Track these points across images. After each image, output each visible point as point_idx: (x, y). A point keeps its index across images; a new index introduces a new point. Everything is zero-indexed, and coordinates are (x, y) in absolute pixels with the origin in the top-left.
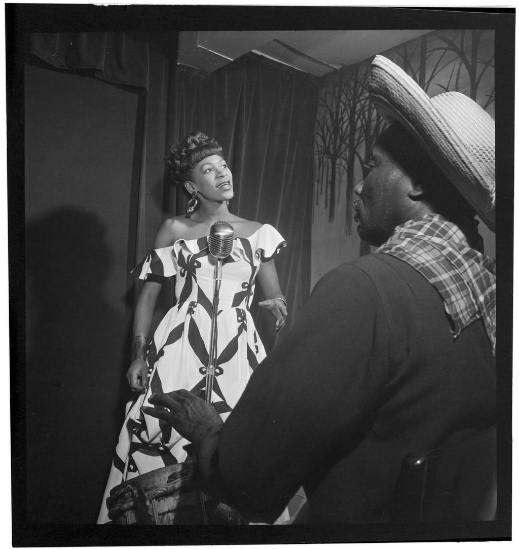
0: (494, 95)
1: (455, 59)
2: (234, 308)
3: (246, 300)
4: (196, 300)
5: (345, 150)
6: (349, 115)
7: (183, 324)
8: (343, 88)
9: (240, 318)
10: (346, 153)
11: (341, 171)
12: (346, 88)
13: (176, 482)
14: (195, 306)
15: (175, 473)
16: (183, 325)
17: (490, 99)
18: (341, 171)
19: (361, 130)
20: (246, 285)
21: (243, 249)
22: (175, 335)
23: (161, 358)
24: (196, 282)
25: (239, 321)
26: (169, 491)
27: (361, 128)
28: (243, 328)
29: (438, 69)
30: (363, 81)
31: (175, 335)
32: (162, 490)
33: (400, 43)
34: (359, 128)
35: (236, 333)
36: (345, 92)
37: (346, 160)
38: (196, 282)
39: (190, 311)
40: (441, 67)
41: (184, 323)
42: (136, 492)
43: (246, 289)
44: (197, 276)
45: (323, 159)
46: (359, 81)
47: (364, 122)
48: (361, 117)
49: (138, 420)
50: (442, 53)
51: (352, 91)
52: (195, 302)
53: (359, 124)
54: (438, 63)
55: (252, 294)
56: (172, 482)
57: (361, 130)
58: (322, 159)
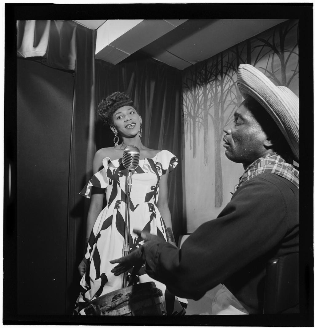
0: (298, 70)
1: (270, 51)
2: (147, 203)
3: (154, 199)
4: (120, 199)
5: (201, 112)
6: (203, 91)
7: (112, 216)
8: (198, 75)
9: (151, 209)
10: (202, 114)
11: (200, 125)
12: (200, 75)
13: (116, 301)
14: (120, 203)
15: (116, 296)
16: (111, 217)
17: (295, 72)
18: (200, 125)
19: (211, 100)
20: (154, 188)
21: (149, 165)
22: (107, 224)
23: (99, 239)
24: (120, 187)
25: (150, 211)
26: (113, 307)
27: (211, 98)
28: (153, 216)
29: (259, 58)
30: (211, 70)
31: (107, 224)
32: (109, 306)
33: (233, 45)
34: (209, 99)
35: (149, 220)
36: (199, 77)
37: (202, 119)
38: (120, 187)
39: (117, 207)
40: (261, 57)
41: (112, 215)
42: (95, 308)
43: (153, 190)
44: (120, 182)
45: (187, 119)
46: (208, 70)
47: (213, 94)
48: (211, 91)
49: (85, 286)
50: (261, 49)
51: (204, 77)
52: (119, 201)
53: (210, 96)
54: (259, 54)
55: (158, 194)
56: (115, 301)
57: (211, 100)
58: (186, 119)
